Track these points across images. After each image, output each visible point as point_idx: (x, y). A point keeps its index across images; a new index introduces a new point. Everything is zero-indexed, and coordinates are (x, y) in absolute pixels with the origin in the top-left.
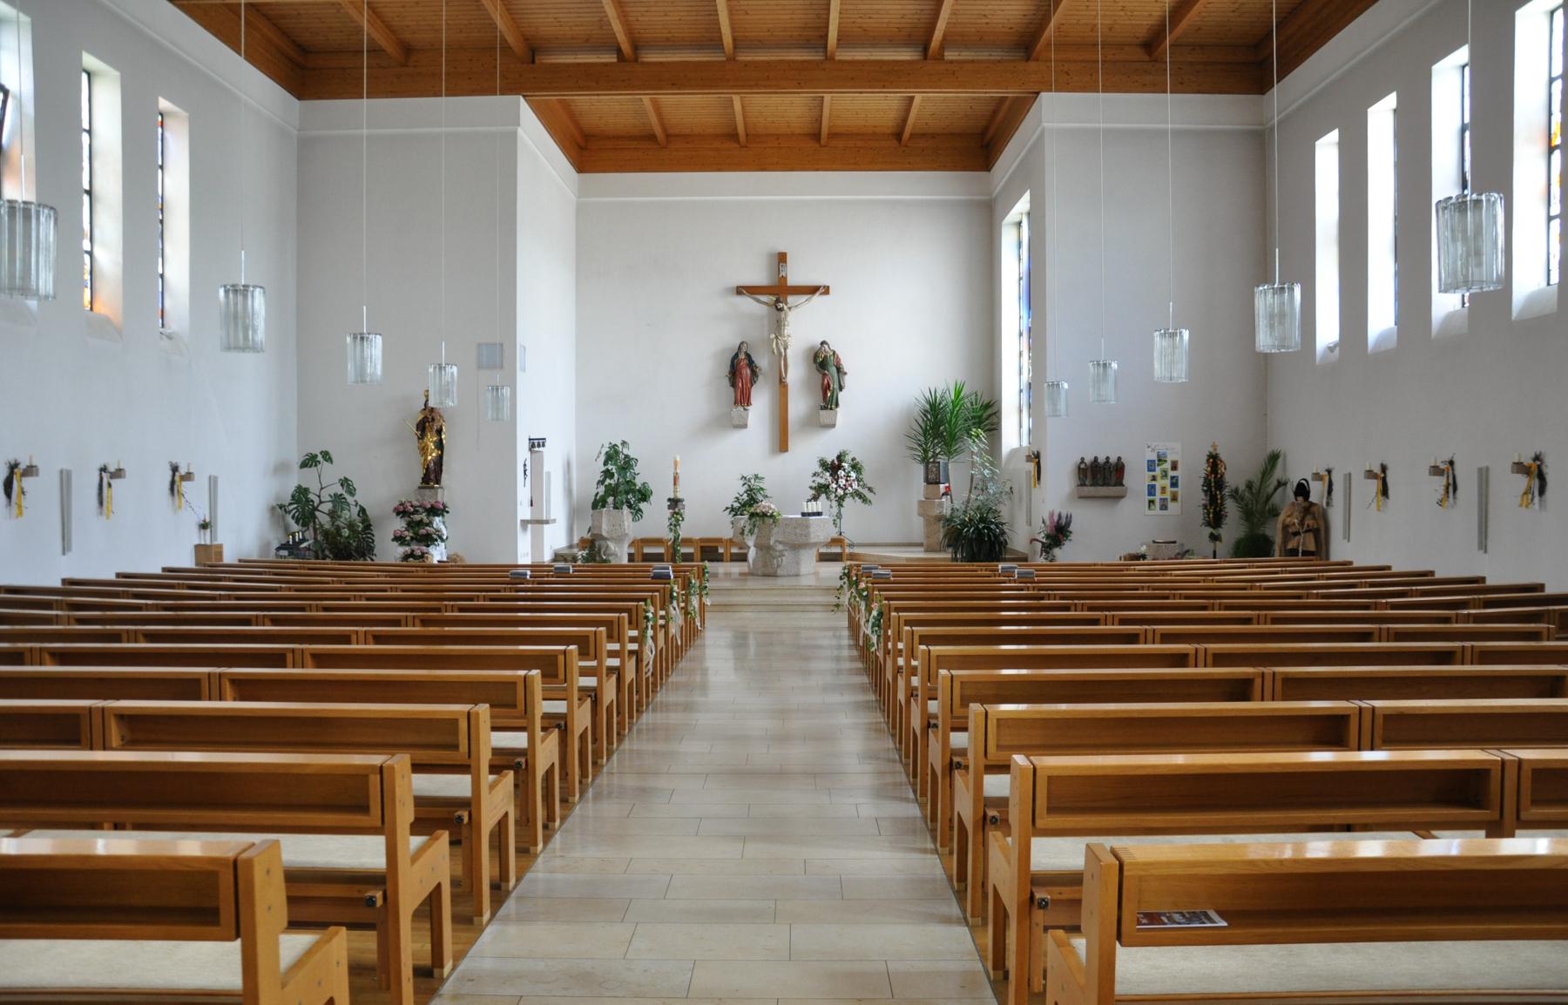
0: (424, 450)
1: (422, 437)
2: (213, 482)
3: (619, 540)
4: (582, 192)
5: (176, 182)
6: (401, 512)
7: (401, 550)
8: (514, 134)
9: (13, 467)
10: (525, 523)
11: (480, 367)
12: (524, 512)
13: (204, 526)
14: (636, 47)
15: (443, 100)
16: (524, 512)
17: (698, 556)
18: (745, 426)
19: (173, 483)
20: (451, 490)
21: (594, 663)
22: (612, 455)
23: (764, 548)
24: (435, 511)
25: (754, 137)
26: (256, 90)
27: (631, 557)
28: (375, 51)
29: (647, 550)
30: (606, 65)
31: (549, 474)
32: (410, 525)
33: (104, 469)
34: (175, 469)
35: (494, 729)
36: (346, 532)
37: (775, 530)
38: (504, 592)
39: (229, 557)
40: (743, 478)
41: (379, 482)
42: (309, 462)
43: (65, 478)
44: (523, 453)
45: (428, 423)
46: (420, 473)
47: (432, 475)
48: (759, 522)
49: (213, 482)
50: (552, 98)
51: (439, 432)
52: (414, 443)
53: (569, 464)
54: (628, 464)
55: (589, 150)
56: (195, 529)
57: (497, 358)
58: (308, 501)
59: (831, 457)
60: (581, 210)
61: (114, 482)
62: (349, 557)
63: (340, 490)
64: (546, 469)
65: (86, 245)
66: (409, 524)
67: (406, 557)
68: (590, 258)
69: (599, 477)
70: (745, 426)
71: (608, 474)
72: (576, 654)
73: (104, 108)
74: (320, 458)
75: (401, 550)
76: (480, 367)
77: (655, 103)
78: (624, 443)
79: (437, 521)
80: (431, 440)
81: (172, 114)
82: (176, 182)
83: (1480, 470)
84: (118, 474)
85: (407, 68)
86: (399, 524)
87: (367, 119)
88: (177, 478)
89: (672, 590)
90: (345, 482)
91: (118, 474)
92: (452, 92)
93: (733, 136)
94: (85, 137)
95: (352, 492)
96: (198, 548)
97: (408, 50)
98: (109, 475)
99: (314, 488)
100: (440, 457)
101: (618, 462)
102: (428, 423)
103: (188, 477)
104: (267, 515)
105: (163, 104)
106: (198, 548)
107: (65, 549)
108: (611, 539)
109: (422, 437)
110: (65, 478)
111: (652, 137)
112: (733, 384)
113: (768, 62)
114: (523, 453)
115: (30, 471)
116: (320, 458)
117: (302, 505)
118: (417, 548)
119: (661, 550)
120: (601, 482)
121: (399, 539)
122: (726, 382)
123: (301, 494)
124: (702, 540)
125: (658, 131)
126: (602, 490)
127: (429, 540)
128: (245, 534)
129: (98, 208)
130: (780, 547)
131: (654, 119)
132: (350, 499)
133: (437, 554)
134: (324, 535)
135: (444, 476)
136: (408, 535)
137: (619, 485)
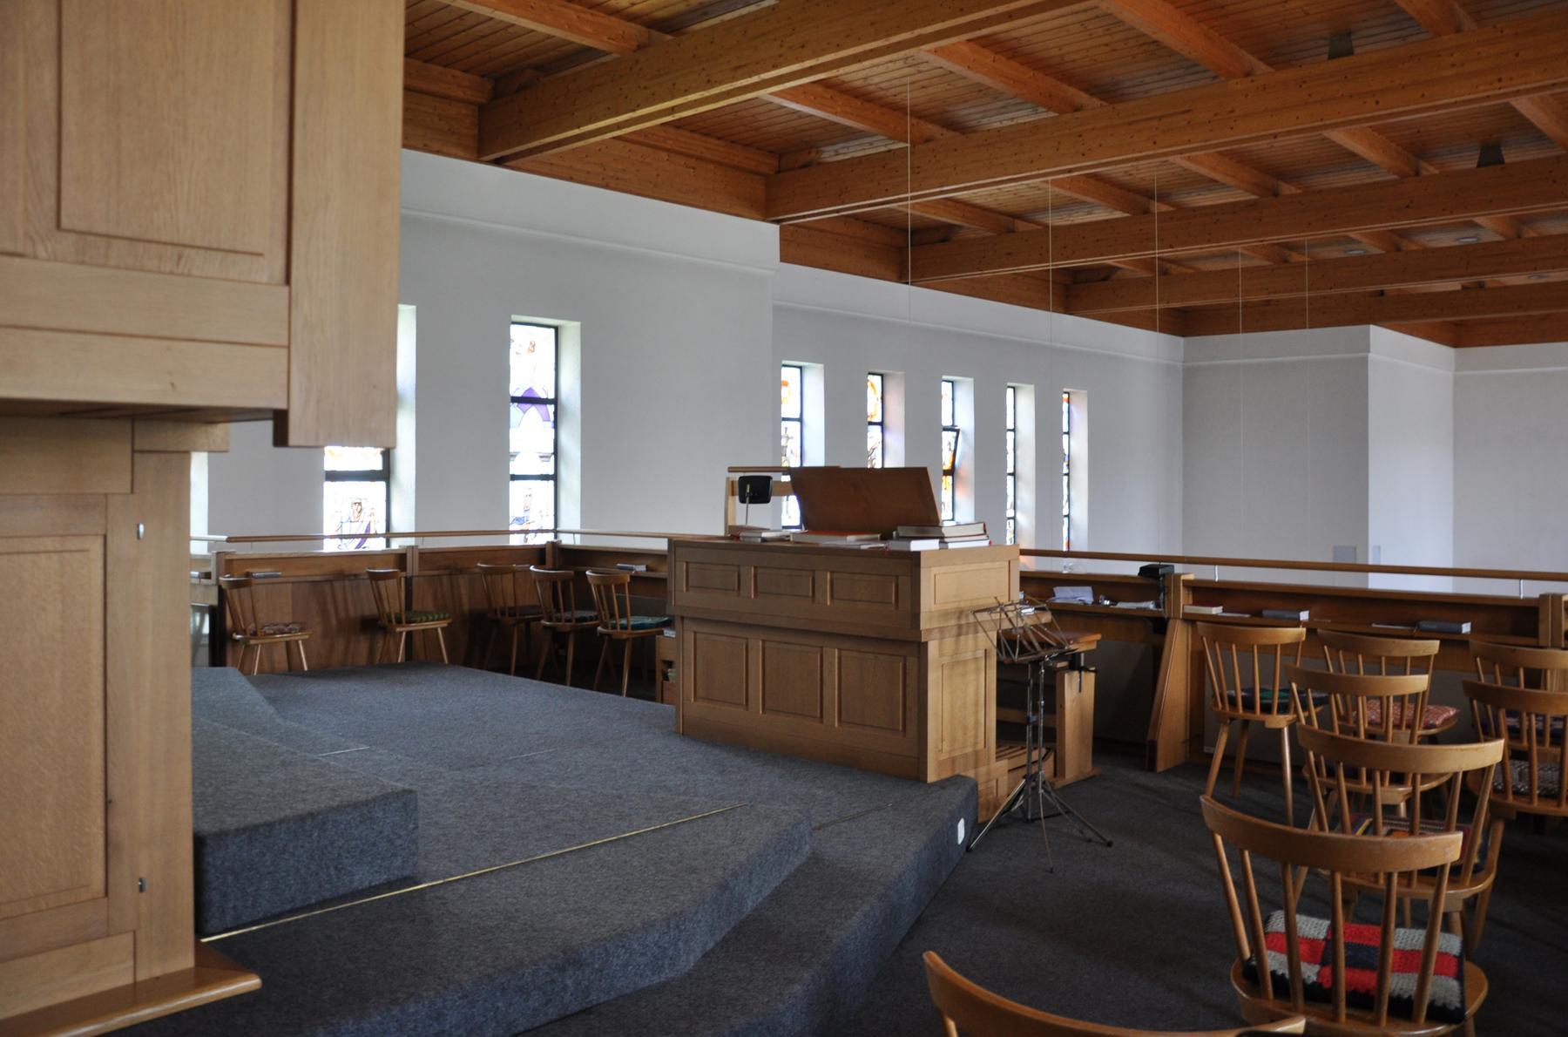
5: (1077, 444)
8: (1365, 361)
60: (1457, 382)
82: (1077, 444)
94: (1010, 436)
129: (1020, 484)
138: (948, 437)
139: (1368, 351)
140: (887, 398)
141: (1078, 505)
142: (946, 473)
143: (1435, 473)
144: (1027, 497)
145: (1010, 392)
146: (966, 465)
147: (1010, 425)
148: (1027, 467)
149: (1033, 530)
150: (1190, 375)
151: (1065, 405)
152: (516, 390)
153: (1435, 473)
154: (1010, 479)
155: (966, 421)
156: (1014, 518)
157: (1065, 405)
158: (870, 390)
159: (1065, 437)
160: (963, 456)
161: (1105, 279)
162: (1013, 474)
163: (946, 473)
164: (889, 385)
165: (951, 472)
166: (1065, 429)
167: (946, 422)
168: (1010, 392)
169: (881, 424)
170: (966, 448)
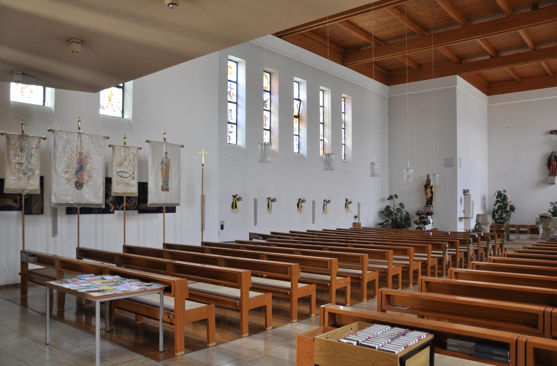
0: (426, 194)
1: (426, 190)
2: (359, 204)
3: (486, 224)
4: (489, 102)
5: (348, 117)
6: (418, 214)
7: (416, 226)
8: (455, 88)
9: (300, 200)
10: (461, 219)
11: (445, 166)
12: (460, 214)
13: (356, 217)
14: (535, 44)
15: (433, 80)
16: (460, 214)
17: (529, 231)
18: (554, 184)
19: (346, 204)
20: (436, 206)
21: (387, 261)
22: (500, 195)
23: (546, 229)
24: (431, 214)
25: (522, 78)
26: (373, 85)
27: (491, 231)
28: (409, 68)
29: (521, 229)
30: (486, 60)
31: (473, 202)
32: (420, 218)
33: (325, 201)
34: (347, 200)
35: (337, 276)
36: (399, 220)
37: (551, 223)
38: (455, 240)
39: (363, 225)
40: (551, 203)
41: (413, 204)
42: (391, 198)
43: (314, 203)
44: (460, 194)
45: (427, 185)
46: (425, 202)
47: (429, 202)
48: (544, 219)
49: (359, 204)
50: (473, 73)
51: (431, 188)
52: (423, 192)
53: (484, 198)
54: (505, 198)
55: (490, 88)
56: (353, 218)
57: (451, 163)
58: (390, 210)
59: (235, 195)
60: (489, 109)
61: (328, 204)
62: (400, 228)
63: (399, 207)
64: (472, 200)
65: (321, 138)
66: (420, 218)
67: (417, 228)
68: (493, 125)
69: (494, 203)
70: (554, 184)
71: (497, 201)
72: (367, 257)
73: (325, 99)
74: (394, 197)
75: (416, 226)
76: (445, 166)
77: (548, 65)
78: (505, 191)
79: (429, 217)
80: (429, 190)
81: (347, 98)
82: (348, 117)
83: (255, 199)
84: (329, 202)
85: (420, 72)
86: (417, 218)
87: (408, 89)
88: (347, 203)
89: (470, 240)
90: (401, 204)
91: (329, 202)
92: (436, 77)
93: (547, 75)
94: (321, 109)
95: (403, 207)
96: (354, 223)
97: (420, 66)
98: (270, 201)
99: (392, 206)
100: (432, 196)
101: (501, 197)
102: (427, 185)
103: (350, 203)
104: (377, 214)
105: (344, 95)
106: (354, 223)
107: (313, 222)
108: (483, 224)
109: (426, 190)
110: (314, 203)
111: (513, 80)
112: (549, 168)
113: (549, 48)
114: (460, 194)
115: (304, 201)
116: (394, 197)
117: (387, 212)
118: (421, 226)
119: (515, 229)
120: (495, 205)
121: (416, 223)
122: (546, 167)
123: (388, 208)
124: (531, 226)
125: (515, 77)
126: (496, 207)
127: (426, 223)
128: (369, 218)
129: (325, 127)
130: (553, 229)
131: (512, 74)
132: (402, 210)
133: (428, 227)
134: (394, 221)
135: (433, 202)
136: (418, 221)
137: (502, 206)
138: (296, 103)
139: (456, 85)
140: (272, 82)
141: (348, 140)
142: (296, 117)
143: (484, 153)
144: (328, 132)
145: (321, 92)
146: (303, 114)
147: (321, 104)
148: (328, 121)
149: (330, 144)
150: (391, 101)
151: (343, 103)
152: (120, 115)
153: (484, 153)
154: (321, 126)
155: (304, 97)
156: (323, 140)
157: (343, 103)
158: (265, 78)
159: (343, 114)
160: (302, 111)
161: (358, 50)
162: (323, 124)
163: (296, 117)
164: (272, 76)
165: (298, 117)
166: (343, 111)
167: (296, 96)
168: (321, 92)
169: (270, 92)
170: (303, 108)
